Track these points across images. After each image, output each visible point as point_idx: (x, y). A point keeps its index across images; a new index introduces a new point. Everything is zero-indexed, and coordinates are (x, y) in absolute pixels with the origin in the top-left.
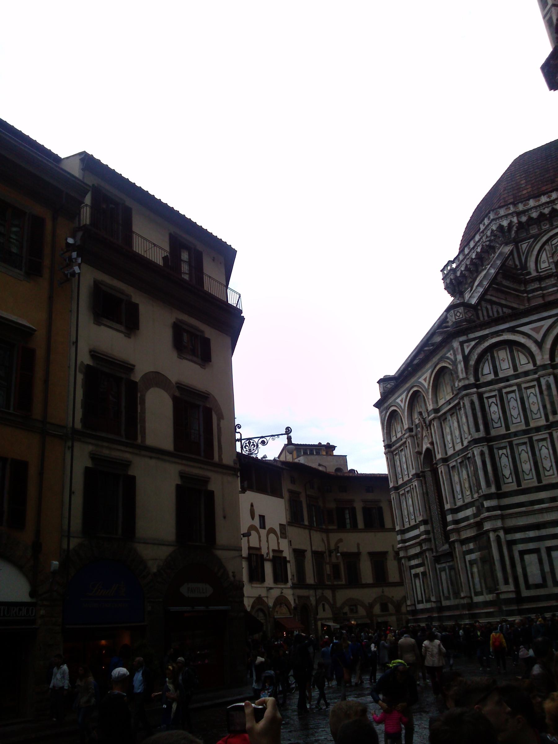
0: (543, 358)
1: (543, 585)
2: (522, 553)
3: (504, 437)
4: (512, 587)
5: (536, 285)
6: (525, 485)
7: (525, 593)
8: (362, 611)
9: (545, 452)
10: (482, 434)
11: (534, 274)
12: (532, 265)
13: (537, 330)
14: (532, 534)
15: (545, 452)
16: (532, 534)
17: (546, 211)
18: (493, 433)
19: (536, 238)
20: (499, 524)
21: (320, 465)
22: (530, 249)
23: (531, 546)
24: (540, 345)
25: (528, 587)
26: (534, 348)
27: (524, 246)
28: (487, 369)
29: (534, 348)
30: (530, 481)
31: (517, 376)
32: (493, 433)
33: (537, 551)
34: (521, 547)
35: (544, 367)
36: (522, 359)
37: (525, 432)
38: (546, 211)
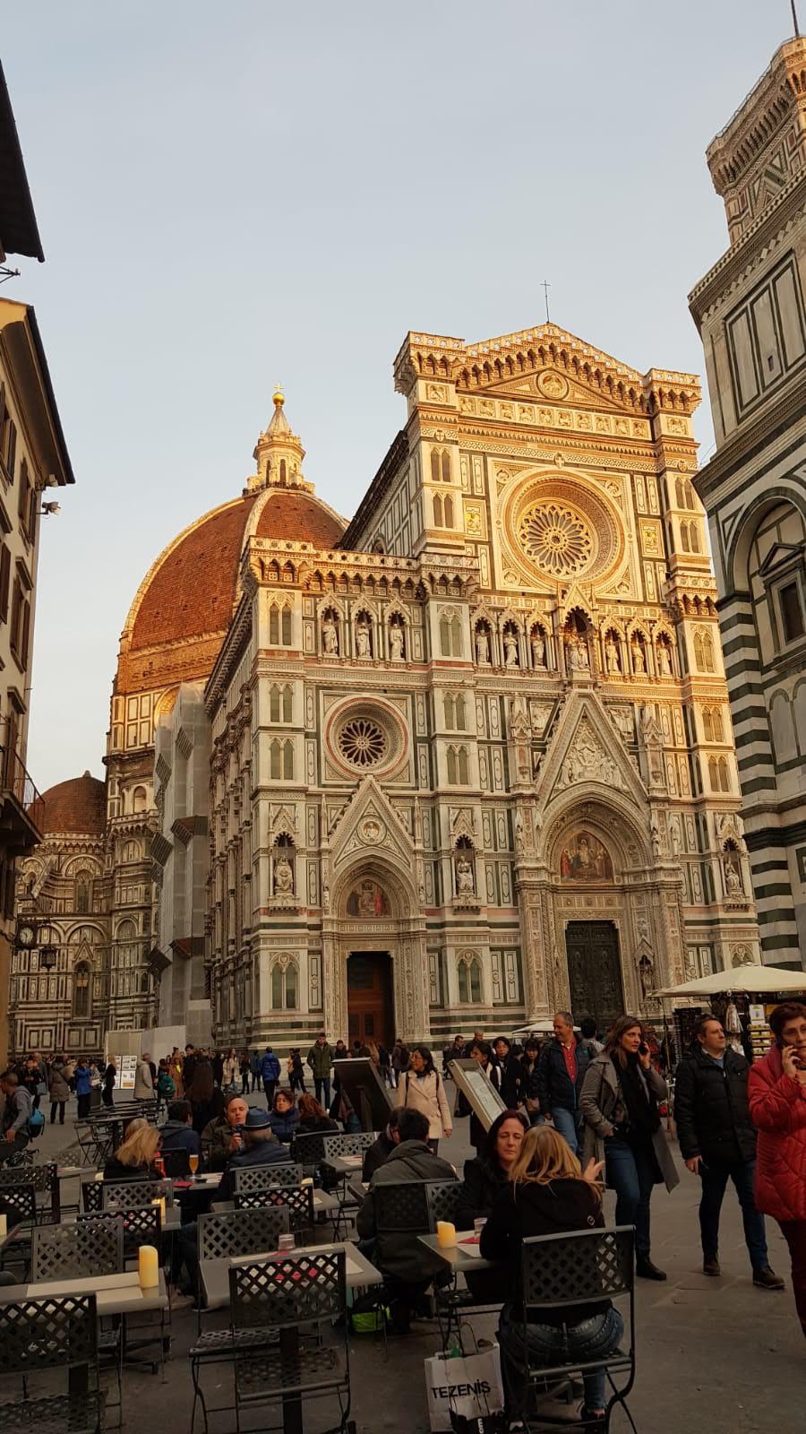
0: (64, 940)
1: (37, 1047)
2: (31, 1031)
3: (36, 974)
5: (63, 883)
6: (40, 999)
8: (522, 1110)
9: (53, 985)
10: (26, 971)
11: (64, 877)
12: (64, 870)
14: (37, 1023)
15: (53, 985)
16: (37, 1023)
17: (81, 844)
18: (31, 971)
19: (71, 855)
21: (763, 1278)
22: (66, 860)
23: (36, 1028)
24: (65, 933)
26: (62, 934)
27: (63, 858)
29: (62, 934)
30: (42, 997)
32: (31, 971)
33: (37, 1031)
34: (32, 1028)
35: (64, 945)
36: (54, 937)
38: (81, 844)
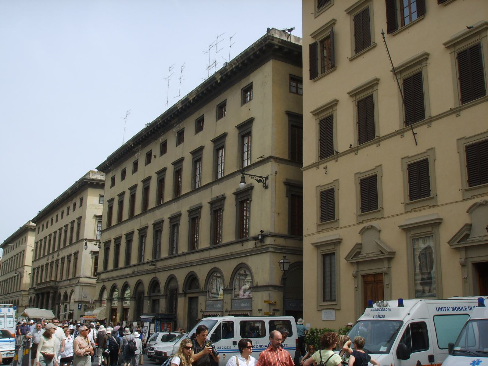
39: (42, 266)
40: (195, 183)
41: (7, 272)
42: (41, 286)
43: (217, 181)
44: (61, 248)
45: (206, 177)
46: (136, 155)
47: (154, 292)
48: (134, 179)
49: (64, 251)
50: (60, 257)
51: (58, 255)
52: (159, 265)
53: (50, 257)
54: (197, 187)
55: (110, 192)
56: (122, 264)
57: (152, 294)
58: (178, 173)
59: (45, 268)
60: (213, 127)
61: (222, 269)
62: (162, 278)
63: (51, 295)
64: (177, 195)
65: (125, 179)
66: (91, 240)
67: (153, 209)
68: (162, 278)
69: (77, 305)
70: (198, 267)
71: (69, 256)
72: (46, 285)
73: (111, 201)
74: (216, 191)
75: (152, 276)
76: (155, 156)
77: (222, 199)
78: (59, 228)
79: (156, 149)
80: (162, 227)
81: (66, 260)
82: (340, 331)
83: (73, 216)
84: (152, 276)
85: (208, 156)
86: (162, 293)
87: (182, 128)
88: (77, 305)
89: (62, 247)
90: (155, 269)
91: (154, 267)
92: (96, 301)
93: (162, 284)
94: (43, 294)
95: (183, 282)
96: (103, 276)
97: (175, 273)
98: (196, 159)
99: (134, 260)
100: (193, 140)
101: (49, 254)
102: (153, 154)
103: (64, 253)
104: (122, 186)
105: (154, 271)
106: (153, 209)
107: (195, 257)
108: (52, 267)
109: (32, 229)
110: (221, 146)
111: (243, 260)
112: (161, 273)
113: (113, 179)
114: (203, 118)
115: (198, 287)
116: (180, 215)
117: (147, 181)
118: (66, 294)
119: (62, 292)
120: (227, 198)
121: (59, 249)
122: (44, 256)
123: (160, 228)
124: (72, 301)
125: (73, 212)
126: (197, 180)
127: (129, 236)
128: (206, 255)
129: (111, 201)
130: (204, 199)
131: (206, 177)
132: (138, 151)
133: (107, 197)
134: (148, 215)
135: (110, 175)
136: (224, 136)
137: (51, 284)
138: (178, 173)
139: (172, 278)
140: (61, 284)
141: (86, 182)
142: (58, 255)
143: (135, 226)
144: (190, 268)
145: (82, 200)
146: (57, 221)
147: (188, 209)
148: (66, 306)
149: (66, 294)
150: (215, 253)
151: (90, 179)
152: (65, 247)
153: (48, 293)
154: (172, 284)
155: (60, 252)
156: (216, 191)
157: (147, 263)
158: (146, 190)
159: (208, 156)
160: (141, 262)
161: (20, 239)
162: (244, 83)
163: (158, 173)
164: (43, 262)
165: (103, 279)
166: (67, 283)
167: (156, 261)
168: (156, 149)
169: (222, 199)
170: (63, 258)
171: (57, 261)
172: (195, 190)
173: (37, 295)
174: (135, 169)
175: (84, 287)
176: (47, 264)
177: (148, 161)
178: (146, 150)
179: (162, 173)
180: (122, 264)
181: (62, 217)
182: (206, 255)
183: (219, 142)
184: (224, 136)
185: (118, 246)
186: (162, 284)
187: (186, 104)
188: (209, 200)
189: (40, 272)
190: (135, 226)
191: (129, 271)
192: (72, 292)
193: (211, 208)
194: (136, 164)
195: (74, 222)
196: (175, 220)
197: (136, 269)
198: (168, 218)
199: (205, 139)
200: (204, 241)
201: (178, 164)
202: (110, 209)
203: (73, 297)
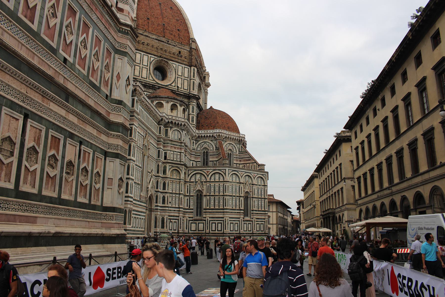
4: (187, 230)
7: (190, 232)
13: (242, 173)
20: (168, 214)
25: (191, 230)
28: (213, 178)
31: (190, 182)
37: (222, 195)
39: (325, 200)
40: (410, 122)
41: (336, 183)
42: (325, 213)
43: (425, 116)
44: (381, 148)
45: (417, 115)
46: (367, 112)
47: (393, 210)
48: (368, 129)
49: (335, 188)
50: (334, 192)
51: (332, 191)
52: (394, 189)
53: (328, 193)
54: (411, 124)
55: (355, 143)
56: (370, 192)
57: (393, 212)
58: (396, 119)
59: (337, 194)
60: (402, 90)
61: (407, 196)
62: (398, 199)
63: (331, 218)
64: (399, 135)
65: (385, 105)
66: (348, 178)
67: (384, 148)
68: (398, 199)
69: (347, 224)
70: (422, 187)
71: (338, 191)
72: (327, 212)
73: (357, 148)
74: (426, 124)
75: (390, 198)
76: (379, 110)
77: (431, 130)
78: (339, 163)
79: (378, 105)
80: (391, 160)
81: (362, 179)
82: (203, 242)
83: (337, 164)
84: (390, 198)
85: (415, 100)
86: (399, 210)
87: (437, 28)
88: (347, 224)
89: (367, 158)
90: (392, 193)
91: (391, 191)
92: (358, 220)
93: (398, 203)
94: (326, 218)
95: (412, 200)
96: (359, 202)
97: (420, 189)
98: (406, 104)
99: (377, 188)
100: (391, 103)
101: (327, 191)
102: (377, 109)
103: (335, 190)
104: (362, 137)
105: (392, 194)
106: (384, 148)
107: (418, 180)
108: (335, 196)
109: (316, 177)
110: (423, 88)
111: (436, 183)
112: (396, 195)
113: (356, 133)
114: (439, 31)
115: (424, 202)
116: (416, 140)
117: (385, 120)
118: (340, 216)
119: (337, 215)
120: (435, 128)
121: (332, 187)
122: (325, 193)
123: (401, 155)
124: (344, 221)
125: (416, 69)
126: (411, 120)
127: (372, 170)
128: (426, 176)
129: (357, 148)
130: (417, 133)
131: (417, 115)
132: (367, 109)
133: (354, 147)
134: (381, 153)
135: (354, 131)
136: (424, 79)
137: (330, 211)
138: (396, 119)
139: (404, 199)
140: (337, 210)
141: (340, 139)
142: (332, 191)
143: (373, 163)
144: (416, 188)
145: (340, 151)
146: (331, 166)
147: (407, 143)
148: (341, 225)
149: (340, 216)
150: (433, 174)
151: (342, 137)
152: (335, 185)
153: (329, 217)
154: (405, 203)
155: (333, 189)
156: (426, 124)
157: (386, 189)
158: (377, 136)
159: (415, 100)
160: (382, 189)
161: (311, 184)
162: (432, 32)
163: (383, 121)
164: (325, 197)
165: (360, 204)
166: (339, 209)
167: (391, 187)
168: (378, 105)
169: (431, 130)
170: (335, 193)
171: (332, 195)
172: (410, 128)
173: (324, 219)
174: (362, 131)
175: (350, 211)
176: (327, 198)
177: (375, 114)
178: (372, 107)
179: (376, 129)
180: (370, 192)
181: (337, 159)
182: (426, 176)
183: (407, 99)
184: (424, 79)
185: (372, 176)
186: (398, 203)
187: (391, 64)
188: (422, 133)
189: (334, 197)
190: (373, 163)
191: (375, 196)
192: (343, 215)
193: (424, 138)
194: (368, 119)
195: (363, 141)
196: (400, 153)
197: (379, 194)
198: (407, 145)
199: (410, 87)
200: (423, 166)
201: (395, 110)
202: (357, 154)
203: (344, 218)
